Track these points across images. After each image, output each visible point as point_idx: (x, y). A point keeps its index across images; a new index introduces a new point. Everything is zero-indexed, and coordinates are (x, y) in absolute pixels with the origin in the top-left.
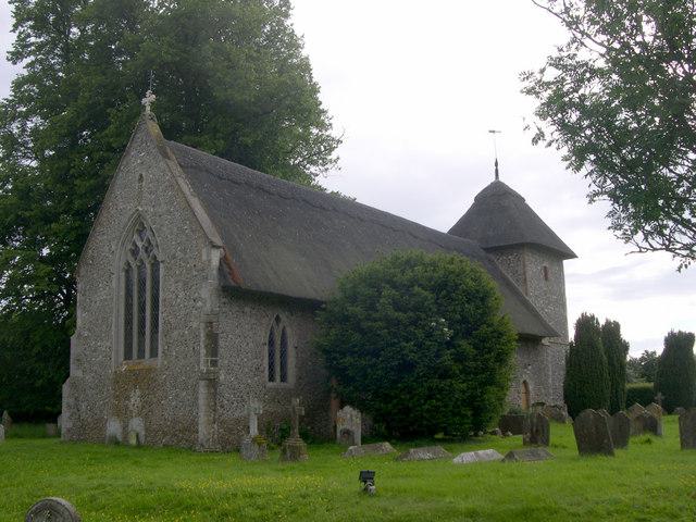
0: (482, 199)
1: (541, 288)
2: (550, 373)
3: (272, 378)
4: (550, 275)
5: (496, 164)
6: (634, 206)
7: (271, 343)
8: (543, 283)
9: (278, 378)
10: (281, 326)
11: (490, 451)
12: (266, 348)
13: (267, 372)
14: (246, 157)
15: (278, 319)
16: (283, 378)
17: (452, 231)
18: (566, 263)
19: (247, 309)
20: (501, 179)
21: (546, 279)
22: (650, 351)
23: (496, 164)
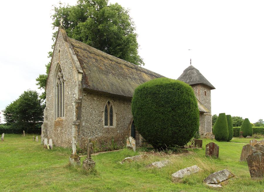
0: (186, 71)
1: (204, 98)
2: (206, 124)
3: (106, 124)
4: (207, 94)
5: (191, 61)
6: (32, 105)
7: (106, 111)
8: (204, 96)
9: (109, 124)
10: (110, 106)
11: (195, 166)
12: (104, 113)
13: (104, 122)
14: (123, 56)
15: (109, 103)
16: (111, 124)
17: (179, 79)
18: (212, 91)
19: (95, 98)
20: (192, 65)
21: (205, 95)
22: (48, 55)
23: (191, 61)
